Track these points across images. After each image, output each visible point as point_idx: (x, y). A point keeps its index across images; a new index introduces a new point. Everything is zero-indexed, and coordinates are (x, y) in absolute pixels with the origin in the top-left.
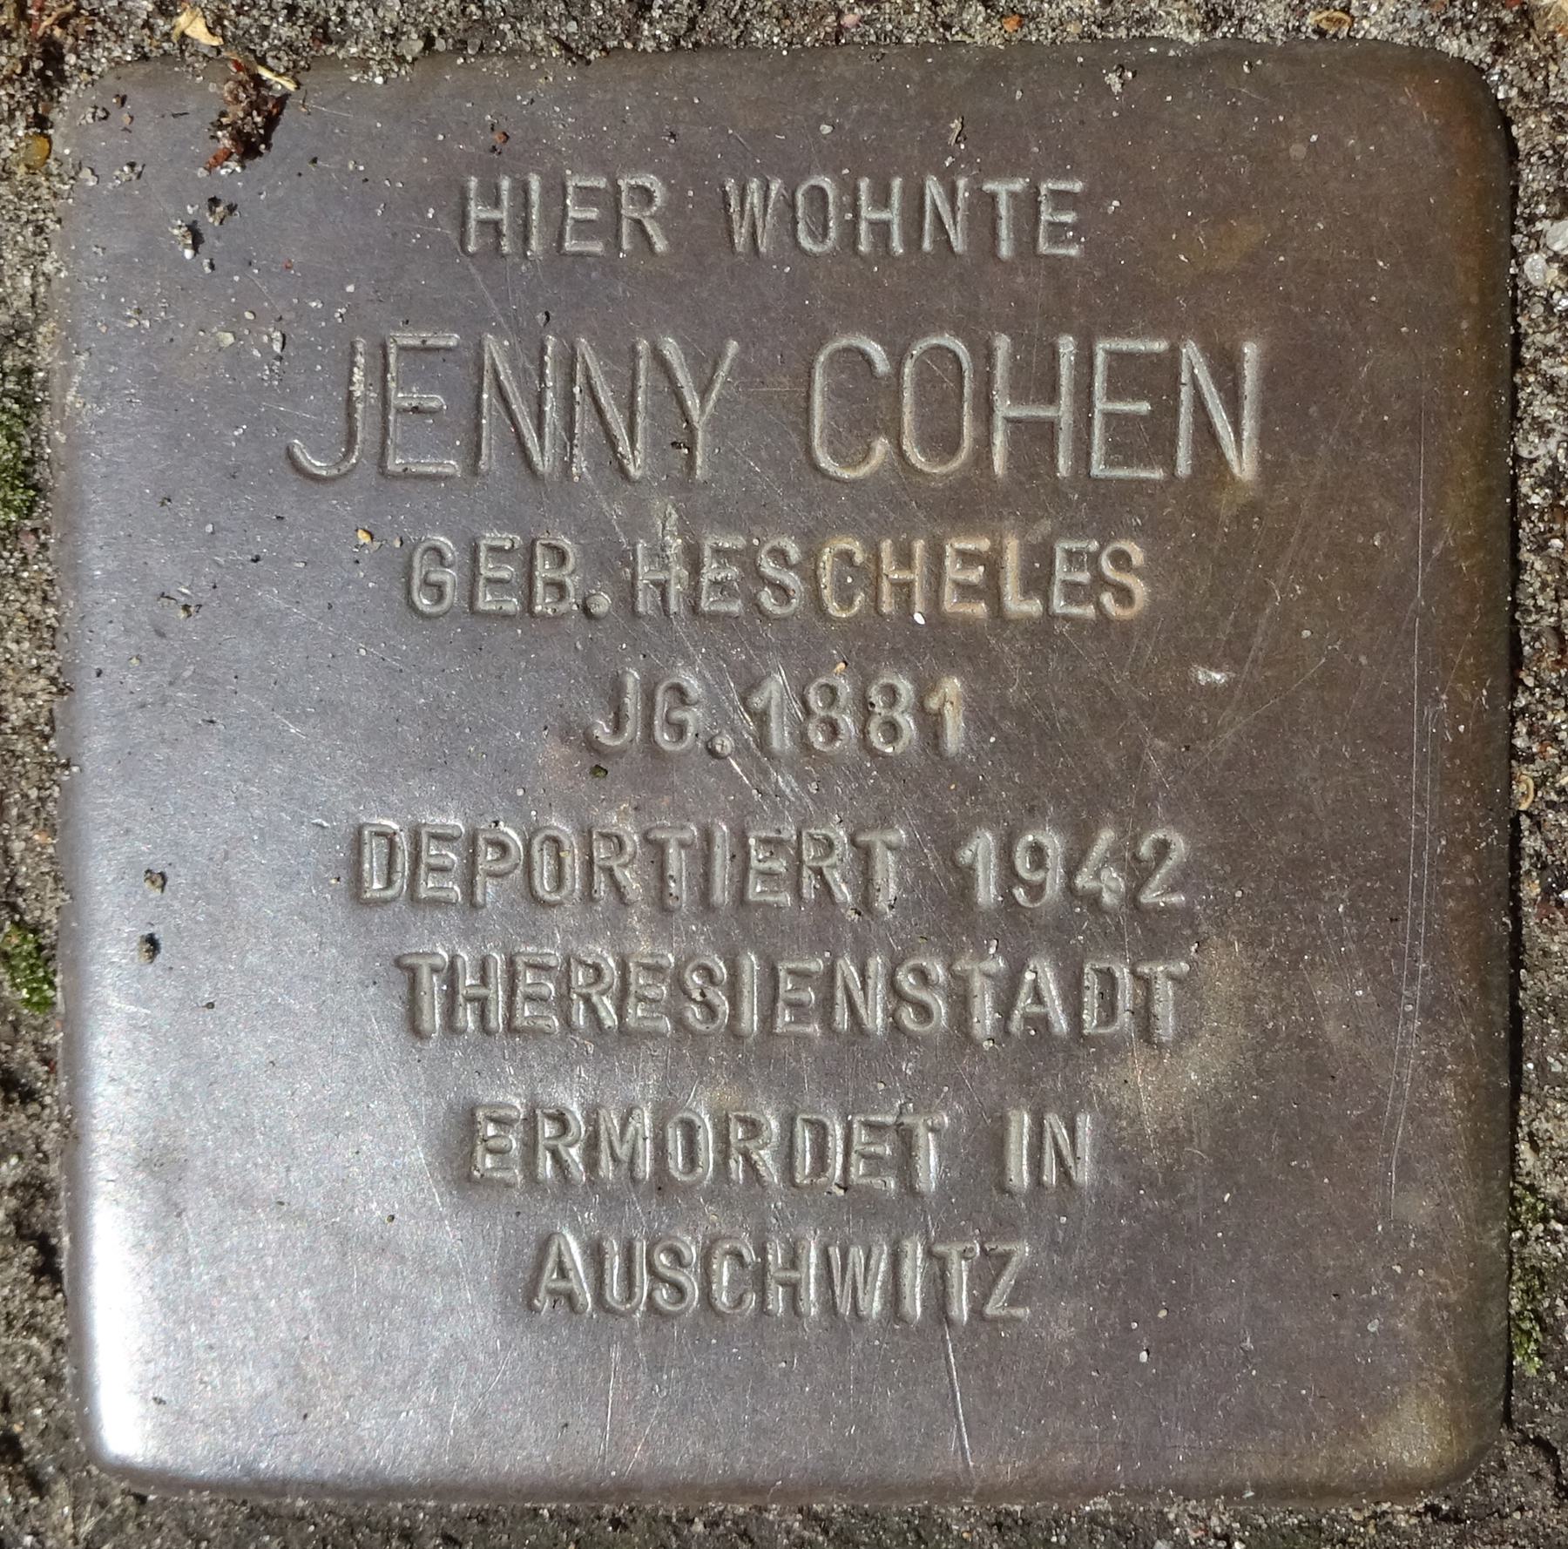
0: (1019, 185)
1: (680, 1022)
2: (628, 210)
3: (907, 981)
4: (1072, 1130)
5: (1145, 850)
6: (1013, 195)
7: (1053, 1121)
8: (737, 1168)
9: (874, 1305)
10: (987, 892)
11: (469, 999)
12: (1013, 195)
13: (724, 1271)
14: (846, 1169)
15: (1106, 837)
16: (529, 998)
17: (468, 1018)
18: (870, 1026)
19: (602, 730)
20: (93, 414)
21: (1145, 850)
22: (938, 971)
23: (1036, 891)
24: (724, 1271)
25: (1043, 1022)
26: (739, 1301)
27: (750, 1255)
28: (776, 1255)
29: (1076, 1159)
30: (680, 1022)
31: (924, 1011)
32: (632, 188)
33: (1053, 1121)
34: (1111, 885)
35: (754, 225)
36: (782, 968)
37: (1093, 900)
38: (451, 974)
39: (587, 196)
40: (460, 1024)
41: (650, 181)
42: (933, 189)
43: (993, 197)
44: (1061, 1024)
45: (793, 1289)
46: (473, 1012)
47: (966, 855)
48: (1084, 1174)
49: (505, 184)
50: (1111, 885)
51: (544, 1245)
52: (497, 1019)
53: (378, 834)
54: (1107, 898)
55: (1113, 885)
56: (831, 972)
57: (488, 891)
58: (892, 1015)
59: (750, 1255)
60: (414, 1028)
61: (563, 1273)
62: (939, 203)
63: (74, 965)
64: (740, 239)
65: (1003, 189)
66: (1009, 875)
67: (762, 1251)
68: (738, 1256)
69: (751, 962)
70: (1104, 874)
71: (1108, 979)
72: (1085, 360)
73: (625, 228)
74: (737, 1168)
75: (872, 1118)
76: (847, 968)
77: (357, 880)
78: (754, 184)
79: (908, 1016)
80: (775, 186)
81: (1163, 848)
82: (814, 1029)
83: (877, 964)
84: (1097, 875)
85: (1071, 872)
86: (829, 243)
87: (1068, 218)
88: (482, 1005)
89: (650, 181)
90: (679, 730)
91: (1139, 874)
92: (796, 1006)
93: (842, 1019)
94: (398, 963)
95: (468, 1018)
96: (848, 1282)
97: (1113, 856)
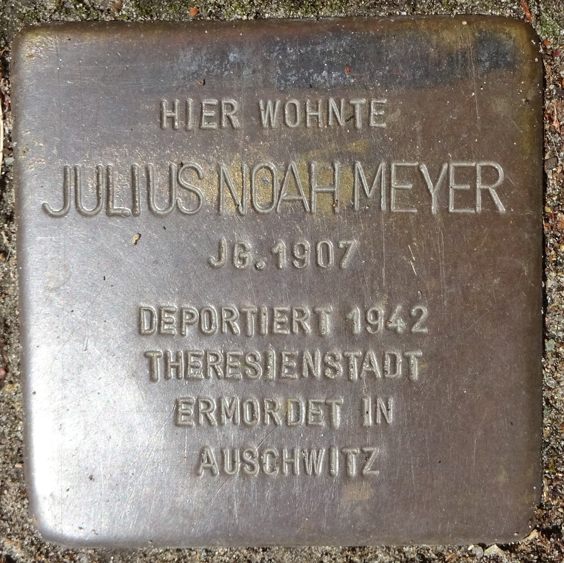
0: (364, 101)
1: (245, 374)
2: (224, 113)
3: (328, 358)
4: (387, 405)
5: (414, 312)
6: (361, 105)
7: (380, 401)
8: (268, 421)
9: (320, 470)
10: (358, 328)
11: (172, 367)
12: (361, 105)
13: (267, 459)
14: (307, 419)
15: (399, 308)
16: (192, 367)
17: (172, 373)
18: (315, 374)
19: (213, 260)
20: (37, 194)
21: (414, 312)
22: (340, 356)
23: (375, 327)
24: (267, 459)
25: (372, 375)
26: (273, 470)
27: (277, 454)
28: (286, 455)
29: (388, 410)
30: (245, 374)
31: (335, 370)
32: (226, 104)
33: (380, 401)
34: (400, 325)
35: (269, 115)
36: (276, 309)
37: (395, 330)
38: (166, 358)
39: (210, 107)
40: (169, 375)
41: (233, 102)
42: (332, 103)
43: (354, 106)
44: (379, 375)
45: (292, 465)
46: (173, 372)
47: (350, 316)
48: (391, 419)
49: (320, 101)
50: (400, 325)
51: (202, 451)
52: (182, 374)
53: (145, 310)
54: (399, 330)
55: (401, 325)
56: (301, 354)
57: (187, 331)
58: (323, 372)
59: (277, 454)
60: (152, 378)
61: (209, 462)
62: (334, 108)
63: (23, 339)
64: (265, 122)
65: (359, 102)
66: (365, 321)
67: (281, 453)
68: (272, 454)
69: (273, 353)
70: (398, 321)
71: (394, 359)
72: (389, 167)
73: (224, 117)
74: (268, 421)
75: (316, 401)
76: (308, 354)
77: (140, 325)
78: (270, 103)
79: (329, 372)
80: (278, 103)
81: (420, 312)
82: (296, 376)
83: (318, 354)
84: (396, 322)
85: (387, 320)
86: (298, 123)
87: (382, 113)
88: (177, 368)
89: (233, 102)
90: (244, 260)
91: (411, 320)
92: (281, 323)
93: (306, 374)
94: (145, 355)
95: (172, 373)
96: (311, 462)
97: (401, 314)
